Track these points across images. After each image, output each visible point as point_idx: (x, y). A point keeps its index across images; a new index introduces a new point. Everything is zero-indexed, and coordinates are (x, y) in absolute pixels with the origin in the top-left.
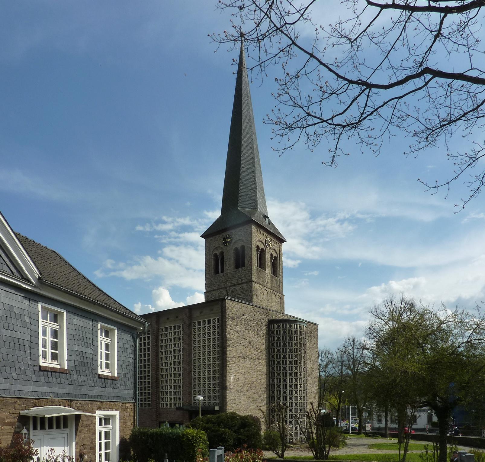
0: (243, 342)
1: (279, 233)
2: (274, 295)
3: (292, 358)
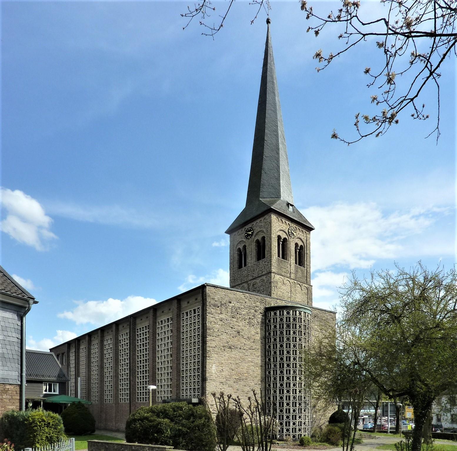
0: (229, 331)
1: (306, 221)
3: (290, 347)
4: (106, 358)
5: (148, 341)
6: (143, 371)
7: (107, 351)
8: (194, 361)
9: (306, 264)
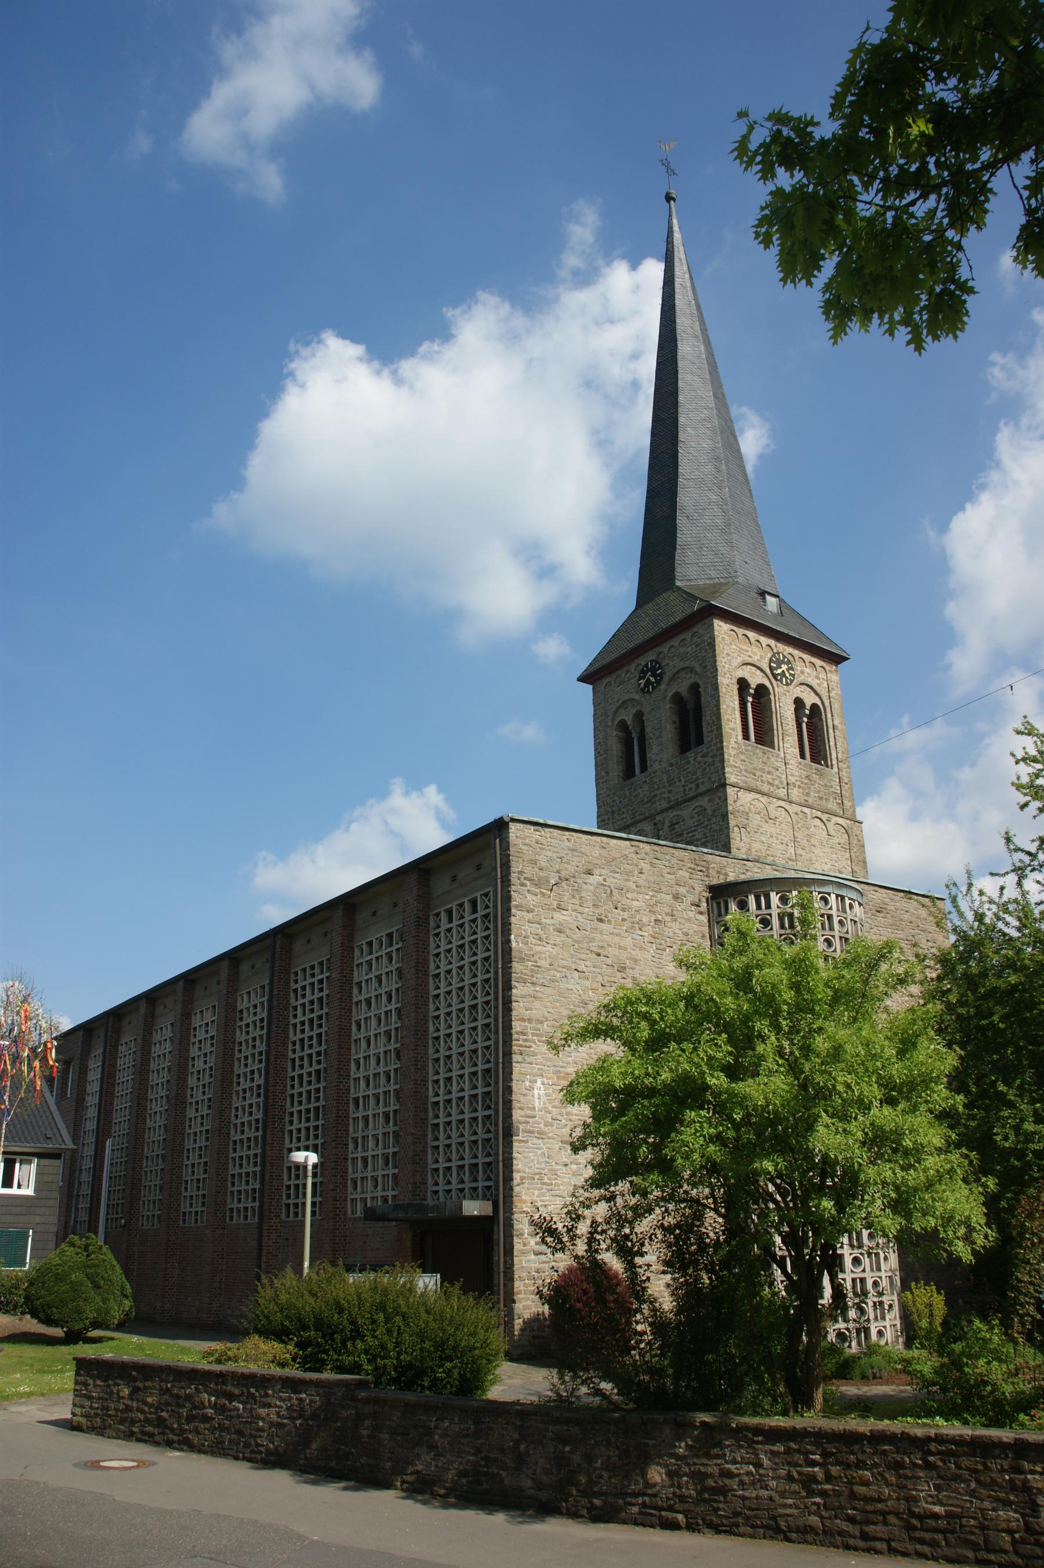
2: (817, 822)
4: (195, 1070)
5: (325, 1010)
6: (308, 1111)
7: (200, 1048)
8: (473, 1069)
9: (834, 756)
